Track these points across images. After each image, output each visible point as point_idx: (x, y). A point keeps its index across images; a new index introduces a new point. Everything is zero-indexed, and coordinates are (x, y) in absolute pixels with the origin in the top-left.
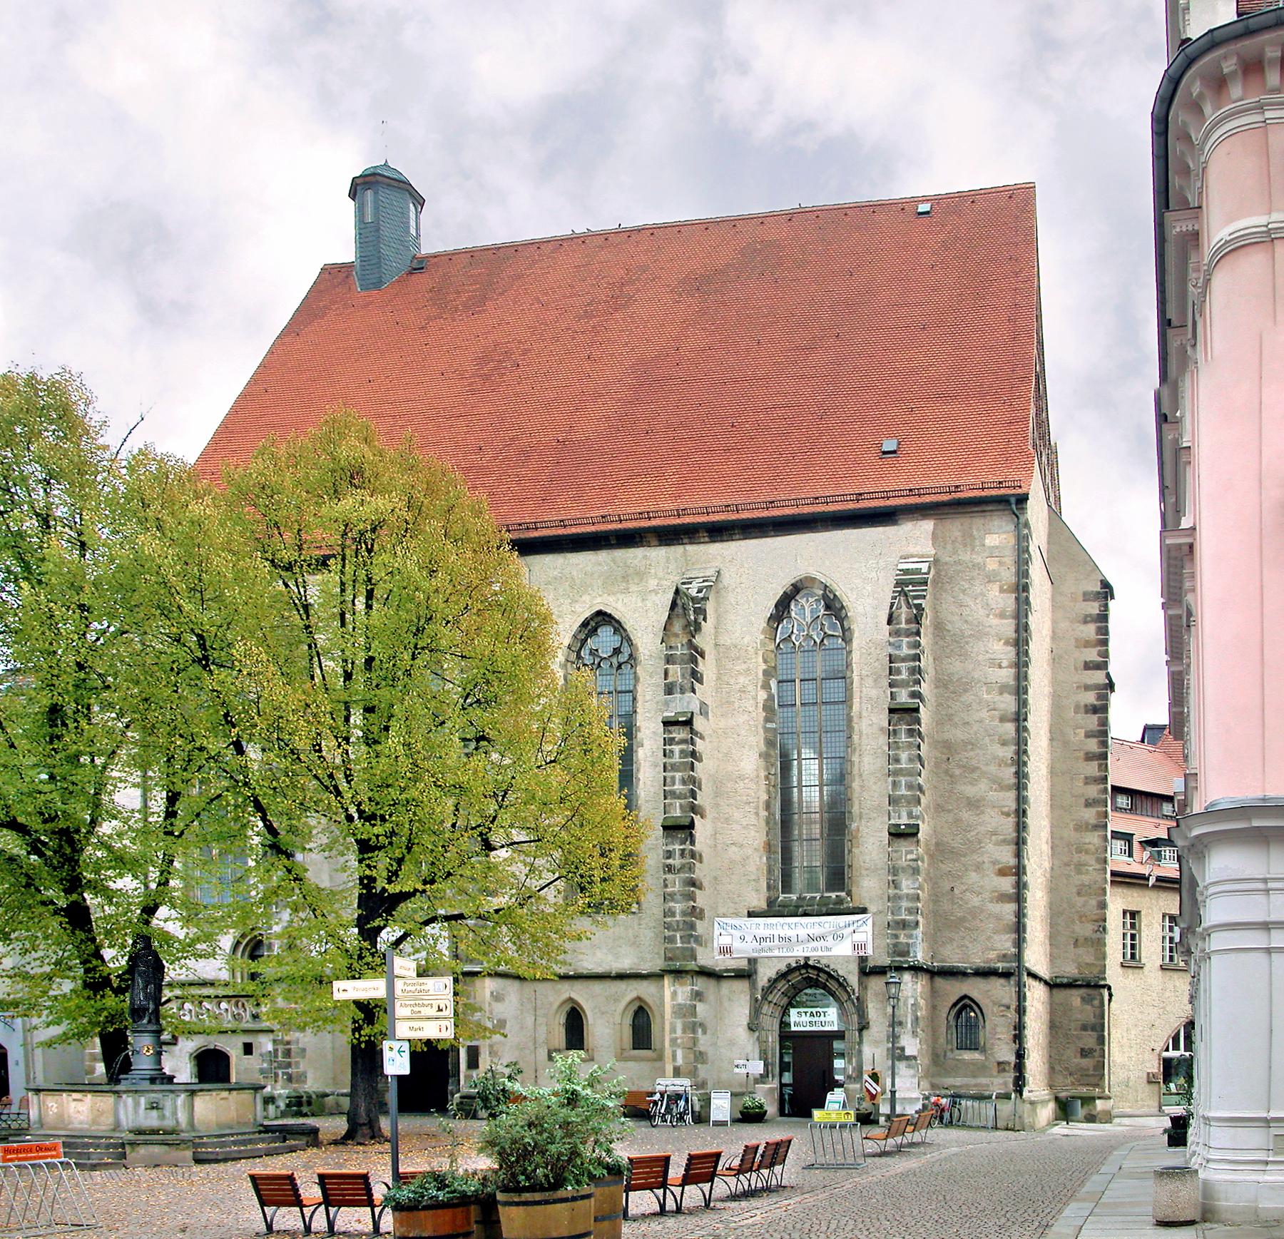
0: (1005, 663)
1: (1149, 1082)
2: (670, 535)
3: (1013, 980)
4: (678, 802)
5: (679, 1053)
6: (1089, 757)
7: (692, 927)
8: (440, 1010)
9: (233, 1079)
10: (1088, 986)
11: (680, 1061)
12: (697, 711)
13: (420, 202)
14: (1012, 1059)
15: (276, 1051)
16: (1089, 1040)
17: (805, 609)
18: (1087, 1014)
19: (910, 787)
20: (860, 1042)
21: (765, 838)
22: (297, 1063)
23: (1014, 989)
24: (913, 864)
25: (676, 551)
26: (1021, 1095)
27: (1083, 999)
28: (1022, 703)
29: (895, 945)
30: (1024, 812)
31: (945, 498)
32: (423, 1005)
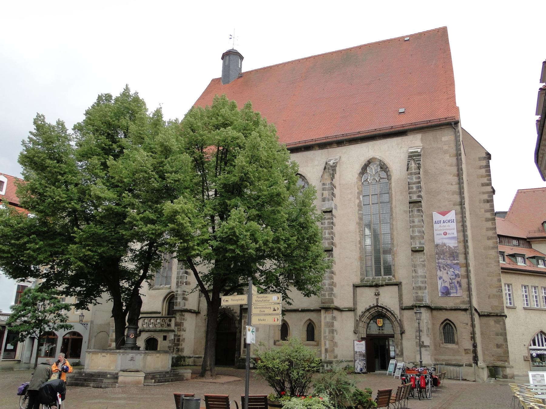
0: (454, 183)
1: (525, 360)
2: (323, 145)
3: (468, 312)
4: (327, 241)
5: (327, 342)
6: (487, 220)
7: (332, 290)
8: (274, 310)
9: (158, 349)
10: (497, 316)
11: (327, 346)
12: (334, 207)
13: (242, 58)
14: (471, 348)
15: (174, 339)
16: (500, 340)
17: (373, 169)
18: (498, 328)
19: (419, 232)
20: (402, 339)
21: (359, 255)
22: (181, 345)
23: (469, 316)
24: (423, 263)
25: (325, 151)
26: (477, 364)
27: (495, 321)
28: (462, 198)
29: (417, 297)
30: (467, 241)
31: (425, 125)
32: (266, 308)
